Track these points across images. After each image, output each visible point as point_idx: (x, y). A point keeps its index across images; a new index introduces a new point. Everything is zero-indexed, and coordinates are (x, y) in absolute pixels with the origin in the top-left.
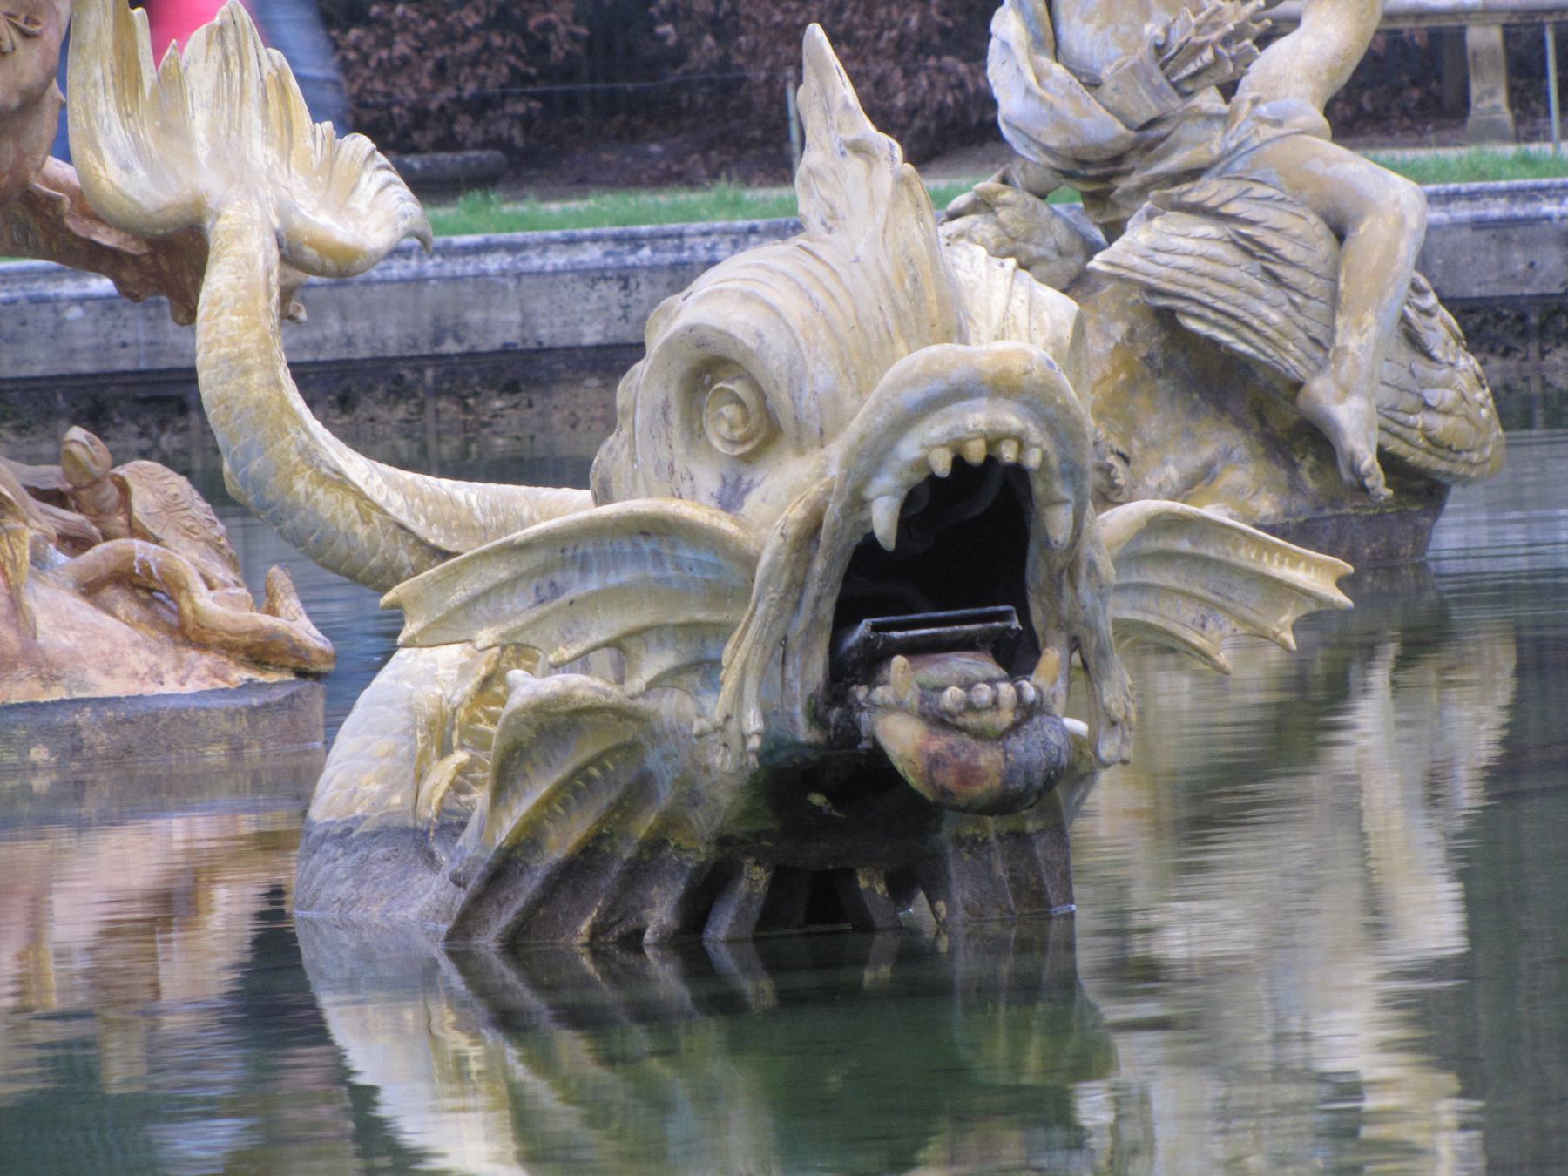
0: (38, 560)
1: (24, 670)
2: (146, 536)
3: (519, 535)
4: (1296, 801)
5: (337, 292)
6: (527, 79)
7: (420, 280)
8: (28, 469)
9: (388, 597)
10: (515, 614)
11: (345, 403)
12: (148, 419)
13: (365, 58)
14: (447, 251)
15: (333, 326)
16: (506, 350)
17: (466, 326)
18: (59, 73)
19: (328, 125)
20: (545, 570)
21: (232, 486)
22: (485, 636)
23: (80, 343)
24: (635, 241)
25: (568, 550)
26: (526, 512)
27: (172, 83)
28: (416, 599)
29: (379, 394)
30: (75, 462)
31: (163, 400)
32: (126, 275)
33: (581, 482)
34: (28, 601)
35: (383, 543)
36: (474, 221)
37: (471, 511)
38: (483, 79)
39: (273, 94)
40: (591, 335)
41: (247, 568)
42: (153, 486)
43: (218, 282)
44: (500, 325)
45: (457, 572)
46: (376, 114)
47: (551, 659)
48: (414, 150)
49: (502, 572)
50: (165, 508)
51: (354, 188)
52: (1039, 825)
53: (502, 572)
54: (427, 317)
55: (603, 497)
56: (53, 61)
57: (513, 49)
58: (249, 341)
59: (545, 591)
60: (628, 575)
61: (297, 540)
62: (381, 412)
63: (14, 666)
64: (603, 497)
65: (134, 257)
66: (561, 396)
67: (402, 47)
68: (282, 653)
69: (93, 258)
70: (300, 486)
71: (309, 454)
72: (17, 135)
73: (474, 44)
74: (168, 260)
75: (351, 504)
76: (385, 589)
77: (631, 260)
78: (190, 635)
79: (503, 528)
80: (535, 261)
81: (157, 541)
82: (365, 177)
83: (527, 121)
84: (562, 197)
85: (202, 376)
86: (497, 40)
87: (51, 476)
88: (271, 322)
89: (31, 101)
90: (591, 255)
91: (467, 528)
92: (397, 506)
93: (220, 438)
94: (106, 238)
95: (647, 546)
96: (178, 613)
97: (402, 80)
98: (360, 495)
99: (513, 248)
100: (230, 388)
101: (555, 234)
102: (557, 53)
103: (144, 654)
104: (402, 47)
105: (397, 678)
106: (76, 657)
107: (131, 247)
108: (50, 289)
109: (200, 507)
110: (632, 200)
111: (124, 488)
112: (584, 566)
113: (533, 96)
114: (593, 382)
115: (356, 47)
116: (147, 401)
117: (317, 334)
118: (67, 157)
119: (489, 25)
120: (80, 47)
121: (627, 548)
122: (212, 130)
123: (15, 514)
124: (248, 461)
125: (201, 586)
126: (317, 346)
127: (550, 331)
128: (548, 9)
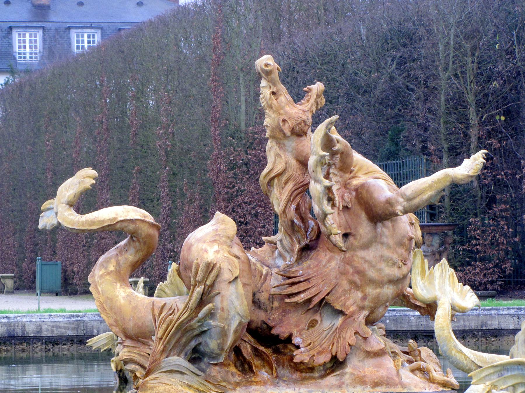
0: (403, 365)
1: (399, 386)
2: (424, 361)
3: (495, 364)
4: (217, 276)
5: (463, 317)
6: (501, 277)
7: (479, 315)
8: (401, 347)
9: (469, 375)
10: (494, 379)
11: (464, 338)
12: (426, 339)
13: (470, 273)
14: (484, 310)
15: (462, 323)
16: (495, 329)
17: (487, 324)
18: (410, 272)
19: (461, 283)
20: (500, 371)
21: (440, 352)
22: (488, 383)
23: (413, 324)
24: (521, 309)
25: (504, 367)
26: (497, 359)
27: (431, 274)
28: (475, 375)
29: (470, 337)
30: (411, 347)
31: (429, 336)
32: (422, 311)
33: (508, 354)
34: (400, 372)
35: (469, 364)
36: (489, 304)
37: (486, 359)
38: (493, 277)
39: (451, 277)
40: (512, 327)
41: (444, 369)
42: (425, 351)
43: (439, 313)
44: (494, 324)
45: (483, 371)
46: (472, 283)
47: (501, 388)
48: (479, 290)
49: (492, 371)
50: (428, 356)
51: (466, 296)
52: (347, 257)
53: (492, 371)
54: (480, 322)
55: (512, 357)
56: (409, 269)
57: (499, 272)
58: (445, 324)
59: (500, 375)
60: (516, 373)
61: (452, 363)
62: (470, 340)
63: (397, 385)
64: (512, 357)
65: (424, 308)
66: (505, 338)
67: (477, 270)
68: (449, 385)
69: (416, 307)
70: (453, 353)
71: (455, 346)
72: (402, 283)
73: (491, 270)
74: (430, 309)
75: (463, 356)
76: (469, 373)
77: (520, 313)
78: (431, 381)
79: (492, 363)
80: (501, 312)
81: (426, 362)
82: (468, 294)
83: (501, 285)
84: (507, 300)
85: (435, 331)
86: (496, 270)
87: (406, 349)
88: (449, 321)
89: (405, 277)
90: (512, 312)
91: (486, 362)
92: (472, 357)
93: (438, 343)
94: (418, 304)
95: (520, 367)
96: (429, 376)
97: (477, 277)
98: (465, 355)
99: (497, 310)
100: (441, 333)
101: (505, 307)
102: (507, 273)
103: (422, 384)
104: (477, 270)
105: (471, 391)
106: (409, 384)
107: (423, 306)
108: (408, 314)
109: (434, 356)
110: (521, 302)
111: (420, 352)
112: (508, 370)
113: (502, 281)
114: (512, 336)
115: (469, 270)
116: (425, 336)
117: (459, 324)
118: (411, 287)
119: (494, 267)
120: (414, 267)
121: (516, 367)
122: (439, 283)
123: (399, 356)
124: (443, 347)
125: (434, 371)
126: (459, 327)
127: (504, 326)
128: (506, 265)
